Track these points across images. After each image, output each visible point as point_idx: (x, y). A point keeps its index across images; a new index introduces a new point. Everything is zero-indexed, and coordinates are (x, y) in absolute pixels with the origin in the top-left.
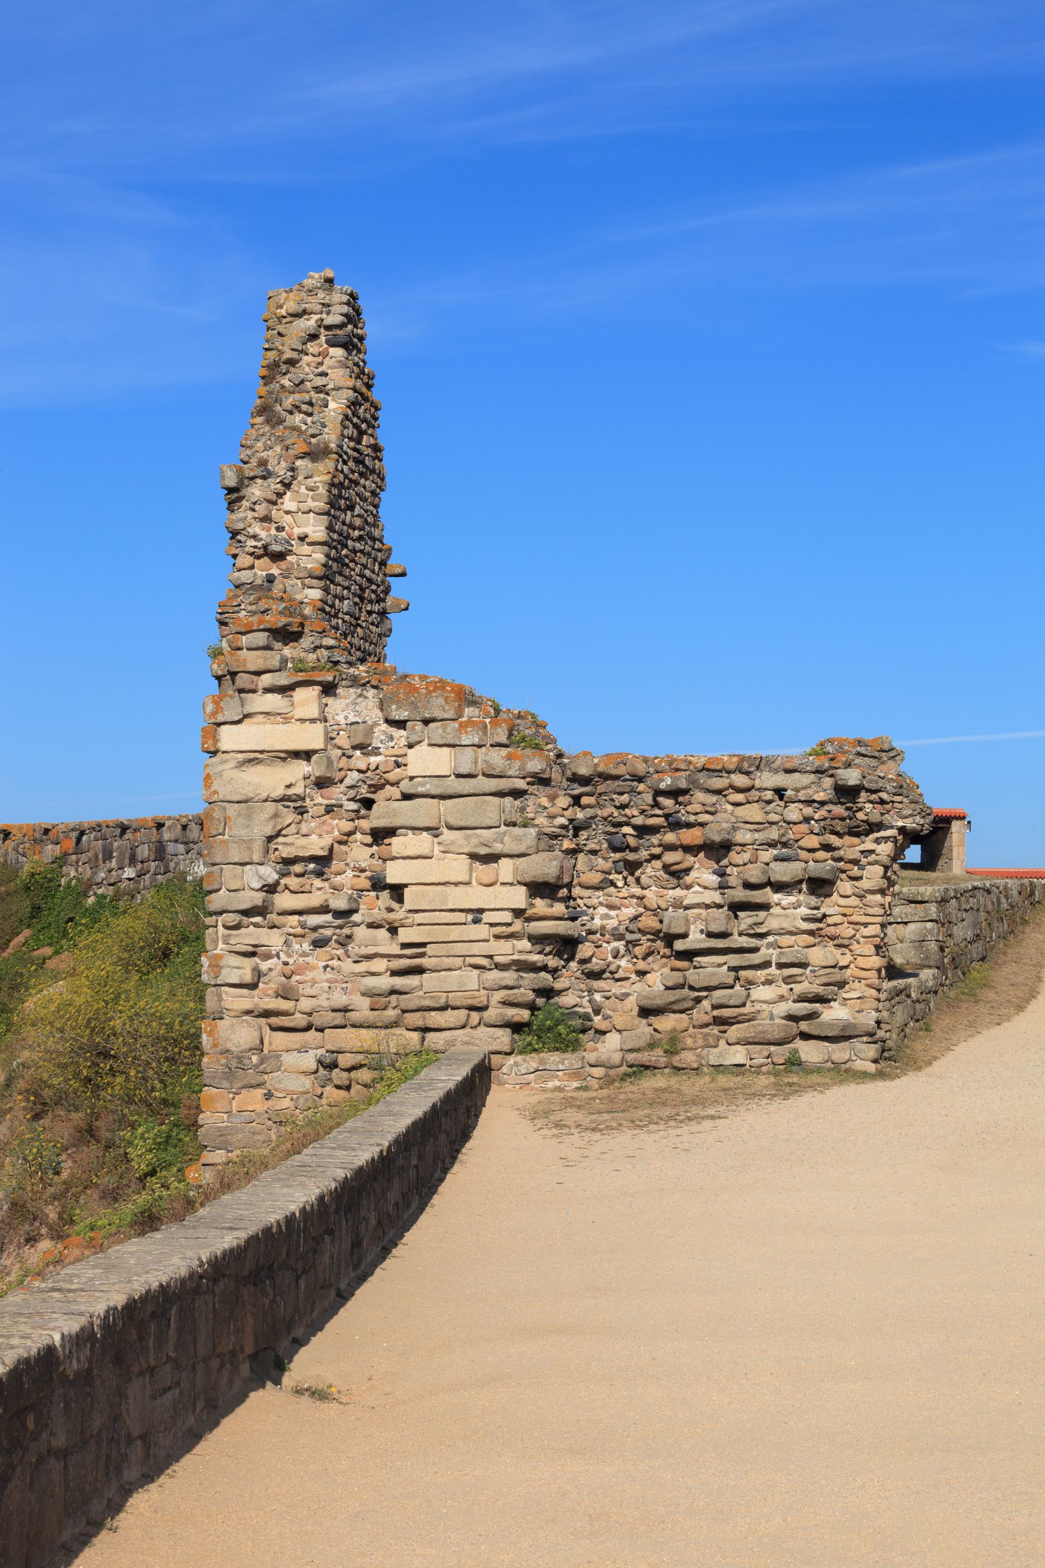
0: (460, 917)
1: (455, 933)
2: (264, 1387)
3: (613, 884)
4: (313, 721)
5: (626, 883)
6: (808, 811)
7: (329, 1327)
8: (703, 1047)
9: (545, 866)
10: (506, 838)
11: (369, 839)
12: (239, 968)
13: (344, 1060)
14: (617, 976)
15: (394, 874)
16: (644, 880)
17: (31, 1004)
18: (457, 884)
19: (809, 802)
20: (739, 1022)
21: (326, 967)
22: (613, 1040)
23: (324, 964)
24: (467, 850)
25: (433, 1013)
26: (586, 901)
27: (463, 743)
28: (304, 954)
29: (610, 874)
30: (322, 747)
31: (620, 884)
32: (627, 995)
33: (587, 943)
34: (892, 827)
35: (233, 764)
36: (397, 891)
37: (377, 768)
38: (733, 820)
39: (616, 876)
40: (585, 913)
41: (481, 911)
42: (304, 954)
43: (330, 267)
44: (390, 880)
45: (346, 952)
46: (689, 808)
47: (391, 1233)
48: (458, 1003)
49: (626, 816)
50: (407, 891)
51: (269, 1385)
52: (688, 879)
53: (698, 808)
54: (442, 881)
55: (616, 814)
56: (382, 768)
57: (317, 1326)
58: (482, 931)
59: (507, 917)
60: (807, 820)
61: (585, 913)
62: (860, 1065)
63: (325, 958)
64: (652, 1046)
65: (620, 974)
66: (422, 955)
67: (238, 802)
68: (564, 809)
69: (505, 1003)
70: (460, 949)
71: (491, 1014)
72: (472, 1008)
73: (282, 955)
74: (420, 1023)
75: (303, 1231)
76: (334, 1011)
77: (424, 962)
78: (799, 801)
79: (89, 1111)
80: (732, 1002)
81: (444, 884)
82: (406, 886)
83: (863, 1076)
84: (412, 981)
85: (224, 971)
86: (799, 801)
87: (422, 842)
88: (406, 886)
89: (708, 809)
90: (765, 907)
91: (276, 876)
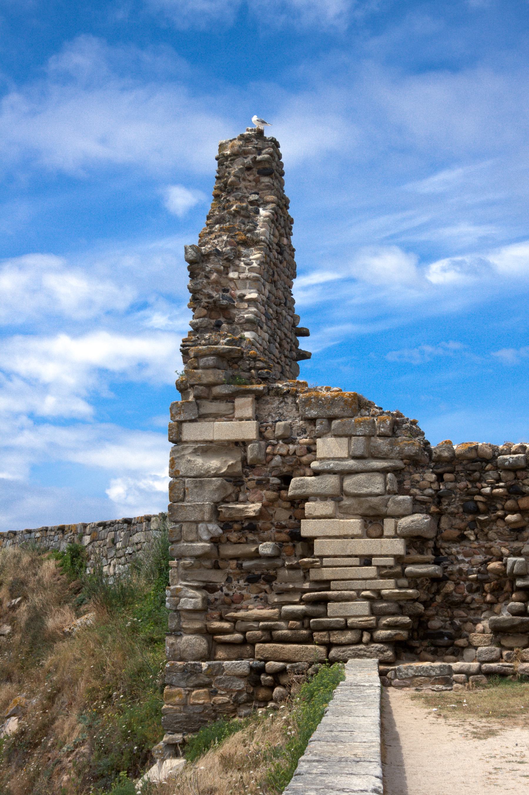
0: (356, 561)
4: (248, 419)
9: (418, 520)
10: (389, 503)
12: (193, 598)
15: (308, 528)
18: (353, 537)
23: (255, 595)
24: (360, 512)
27: (358, 434)
29: (465, 530)
31: (472, 538)
33: (450, 582)
35: (190, 450)
36: (309, 541)
39: (469, 532)
54: (342, 533)
56: (298, 453)
58: (371, 571)
59: (390, 561)
63: (256, 592)
66: (329, 589)
69: (388, 627)
72: (363, 629)
74: (326, 639)
82: (316, 538)
84: (320, 609)
87: (327, 507)
88: (316, 538)
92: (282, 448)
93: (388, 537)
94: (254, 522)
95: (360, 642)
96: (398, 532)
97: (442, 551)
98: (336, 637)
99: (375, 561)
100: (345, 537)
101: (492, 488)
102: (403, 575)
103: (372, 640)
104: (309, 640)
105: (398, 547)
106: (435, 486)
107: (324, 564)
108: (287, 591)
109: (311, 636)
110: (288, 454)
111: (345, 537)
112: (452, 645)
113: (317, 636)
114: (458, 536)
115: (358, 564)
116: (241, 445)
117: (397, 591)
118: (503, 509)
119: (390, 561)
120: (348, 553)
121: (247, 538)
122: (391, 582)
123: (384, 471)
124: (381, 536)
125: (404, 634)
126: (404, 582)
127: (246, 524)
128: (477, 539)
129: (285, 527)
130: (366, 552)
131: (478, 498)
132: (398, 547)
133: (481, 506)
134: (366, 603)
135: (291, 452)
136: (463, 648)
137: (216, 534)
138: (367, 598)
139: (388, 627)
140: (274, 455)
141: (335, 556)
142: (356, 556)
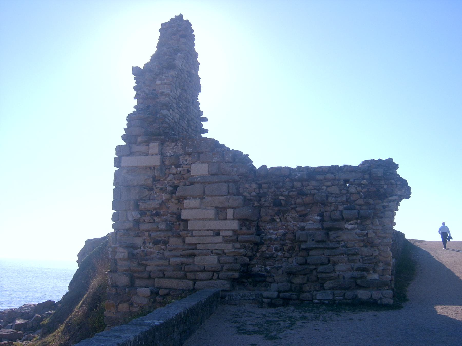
0: (211, 233)
1: (208, 240)
2: (124, 138)
3: (275, 220)
5: (280, 220)
6: (359, 188)
7: (329, 164)
8: (314, 291)
11: (176, 202)
13: (162, 292)
14: (276, 259)
15: (185, 215)
16: (288, 218)
17: (158, 324)
19: (360, 185)
20: (330, 280)
21: (158, 253)
22: (274, 286)
25: (198, 273)
26: (264, 227)
28: (150, 248)
30: (123, 158)
31: (278, 220)
32: (280, 267)
34: (396, 195)
36: (186, 221)
37: (180, 173)
38: (327, 193)
40: (263, 233)
41: (219, 230)
42: (150, 248)
43: (268, 169)
44: (183, 217)
45: (166, 247)
46: (308, 188)
47: (344, 176)
48: (209, 269)
49: (280, 191)
50: (189, 222)
51: (185, 19)
52: (307, 218)
53: (311, 187)
55: (276, 191)
56: (182, 173)
57: (334, 169)
58: (219, 239)
59: (230, 233)
60: (358, 193)
61: (263, 233)
62: (385, 301)
64: (290, 290)
65: (278, 258)
66: (196, 249)
67: (456, 251)
68: (255, 189)
69: (228, 270)
70: (210, 246)
71: (222, 275)
72: (214, 272)
73: (142, 248)
74: (193, 277)
75: (159, 320)
76: (155, 266)
77: (195, 251)
78: (355, 184)
79: (256, 204)
80: (327, 271)
81: (200, 236)
82: (190, 220)
83: (387, 307)
84: (190, 260)
85: (117, 254)
86: (355, 184)
88: (190, 220)
89: (315, 187)
90: (341, 229)
91: (139, 216)
92: (174, 170)
93: (230, 220)
94: (158, 211)
95: (212, 279)
96: (235, 217)
97: (261, 228)
98: (201, 275)
99: (221, 233)
100: (205, 219)
101: (289, 192)
102: (237, 241)
103: (218, 278)
104: (184, 277)
105: (235, 225)
106: (257, 191)
107: (194, 234)
108: (175, 249)
109: (185, 275)
110: (177, 173)
111: (205, 219)
112: (265, 281)
113: (189, 275)
114: (270, 220)
115: (212, 235)
116: (153, 169)
117: (233, 250)
118: (295, 204)
119: (230, 233)
120: (207, 228)
121: (154, 221)
122: (230, 246)
123: (227, 182)
124: (226, 219)
125: (237, 275)
126: (238, 245)
127: (154, 212)
128: (281, 221)
129: (175, 214)
130: (217, 228)
131: (281, 197)
132: (235, 225)
133: (283, 202)
134: (216, 257)
135: (178, 172)
136: (271, 283)
137: (137, 218)
138: (217, 254)
139: (228, 270)
140: (170, 174)
141: (200, 230)
142: (211, 230)
